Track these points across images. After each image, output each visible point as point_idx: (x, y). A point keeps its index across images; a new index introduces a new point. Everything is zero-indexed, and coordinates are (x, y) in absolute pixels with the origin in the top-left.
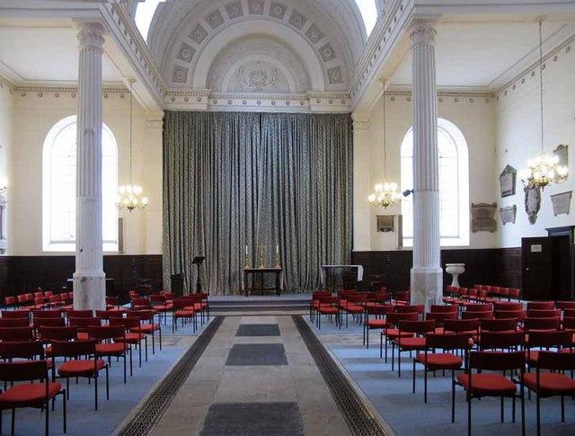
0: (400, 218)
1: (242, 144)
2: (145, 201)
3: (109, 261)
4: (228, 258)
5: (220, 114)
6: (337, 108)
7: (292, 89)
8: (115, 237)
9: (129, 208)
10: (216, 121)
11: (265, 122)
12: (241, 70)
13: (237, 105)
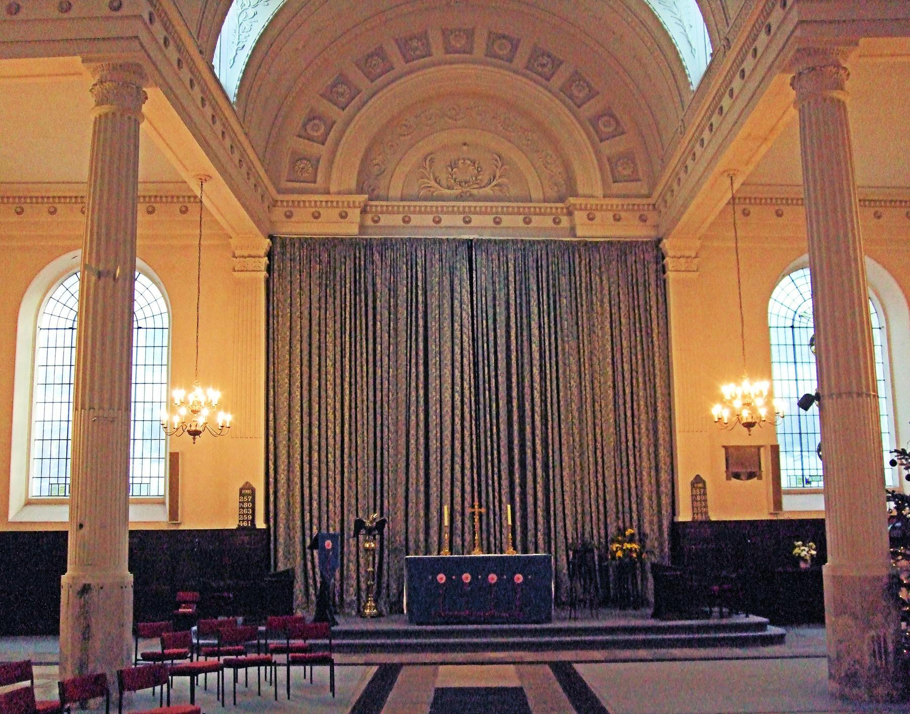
0: (775, 450)
1: (433, 302)
2: (224, 418)
3: (143, 543)
4: (346, 475)
5: (385, 244)
6: (633, 230)
7: (536, 194)
8: (159, 487)
9: (190, 433)
10: (377, 257)
11: (480, 258)
12: (429, 159)
13: (422, 225)
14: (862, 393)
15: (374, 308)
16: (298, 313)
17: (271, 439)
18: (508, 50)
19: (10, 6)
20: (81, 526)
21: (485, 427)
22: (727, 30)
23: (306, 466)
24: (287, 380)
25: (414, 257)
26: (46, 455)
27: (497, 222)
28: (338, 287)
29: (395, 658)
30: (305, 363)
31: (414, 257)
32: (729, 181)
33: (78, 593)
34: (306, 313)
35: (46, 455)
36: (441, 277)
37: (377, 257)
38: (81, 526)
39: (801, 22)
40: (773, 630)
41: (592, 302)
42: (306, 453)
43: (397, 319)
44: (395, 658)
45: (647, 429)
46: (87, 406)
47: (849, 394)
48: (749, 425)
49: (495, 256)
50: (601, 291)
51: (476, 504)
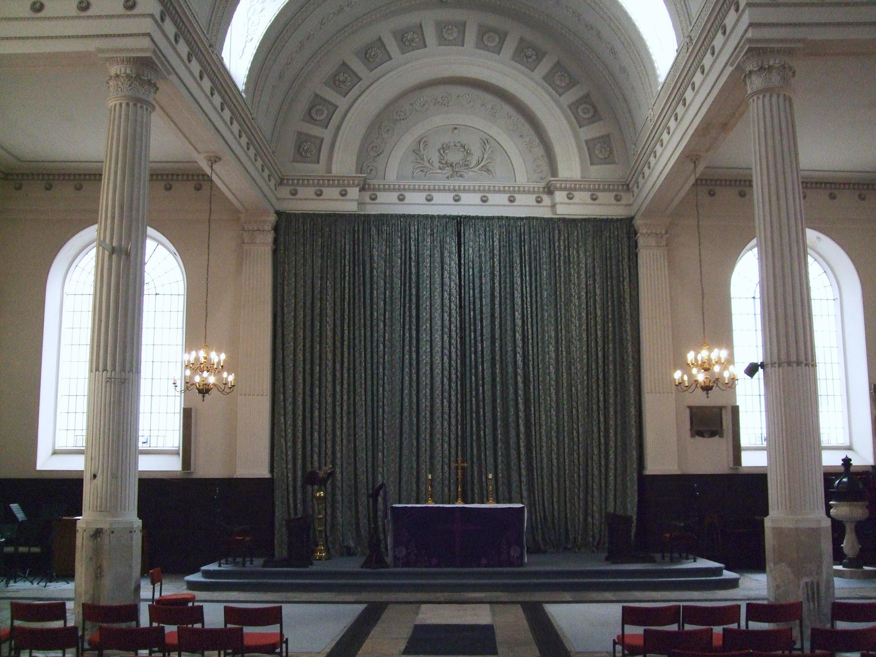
0: (735, 410)
1: (425, 272)
6: (606, 208)
8: (174, 439)
10: (374, 230)
11: (468, 233)
12: (422, 142)
13: (416, 205)
14: (802, 362)
16: (302, 282)
18: (496, 43)
19: (34, 3)
20: (95, 476)
21: (471, 386)
22: (690, 28)
23: (308, 421)
24: (292, 344)
25: (408, 232)
26: (72, 410)
27: (484, 200)
29: (384, 597)
31: (408, 232)
32: (693, 165)
33: (91, 537)
34: (309, 282)
35: (72, 410)
36: (432, 249)
37: (374, 230)
38: (95, 476)
39: (751, 25)
40: (728, 574)
41: (570, 274)
42: (308, 410)
43: (392, 289)
44: (384, 597)
46: (101, 369)
47: (789, 364)
48: (707, 388)
50: (578, 264)
51: (460, 459)
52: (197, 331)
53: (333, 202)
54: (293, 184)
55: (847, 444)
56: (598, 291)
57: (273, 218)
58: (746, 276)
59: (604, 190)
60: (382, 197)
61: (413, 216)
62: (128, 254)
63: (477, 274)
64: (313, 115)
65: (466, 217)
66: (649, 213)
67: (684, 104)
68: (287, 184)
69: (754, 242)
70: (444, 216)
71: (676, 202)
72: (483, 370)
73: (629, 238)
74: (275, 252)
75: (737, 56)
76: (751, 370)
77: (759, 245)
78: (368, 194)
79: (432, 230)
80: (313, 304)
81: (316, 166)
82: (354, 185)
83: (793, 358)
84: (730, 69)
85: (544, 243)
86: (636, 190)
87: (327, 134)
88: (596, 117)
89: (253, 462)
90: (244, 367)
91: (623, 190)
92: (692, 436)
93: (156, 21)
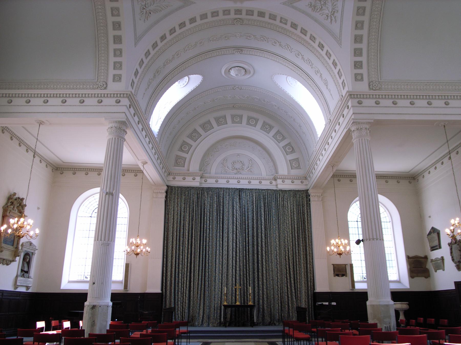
0: (351, 266)
3: (115, 296)
6: (297, 186)
10: (206, 194)
11: (243, 195)
12: (225, 160)
15: (204, 212)
17: (165, 259)
20: (94, 283)
23: (177, 260)
28: (191, 204)
30: (178, 231)
34: (179, 213)
37: (206, 194)
38: (94, 283)
39: (354, 113)
44: (209, 341)
45: (304, 258)
46: (99, 239)
49: (248, 194)
52: (133, 231)
53: (190, 182)
54: (174, 175)
55: (398, 280)
56: (295, 218)
57: (165, 188)
58: (354, 213)
59: (297, 179)
60: (209, 181)
61: (222, 188)
62: (112, 195)
63: (246, 211)
64: (183, 149)
65: (242, 189)
66: (316, 186)
67: (328, 144)
68: (172, 175)
69: (358, 198)
70: (234, 188)
71: (326, 181)
72: (249, 249)
73: (307, 198)
74: (166, 202)
75: (349, 125)
76: (358, 242)
77: (360, 200)
78: (204, 179)
79: (229, 194)
80: (180, 222)
81: (183, 168)
82: (198, 176)
83: (375, 237)
84: (346, 130)
85: (273, 199)
86: (309, 179)
87: (187, 156)
88: (293, 151)
89: (154, 286)
90: (151, 246)
91: (304, 179)
92: (334, 276)
93: (127, 108)
